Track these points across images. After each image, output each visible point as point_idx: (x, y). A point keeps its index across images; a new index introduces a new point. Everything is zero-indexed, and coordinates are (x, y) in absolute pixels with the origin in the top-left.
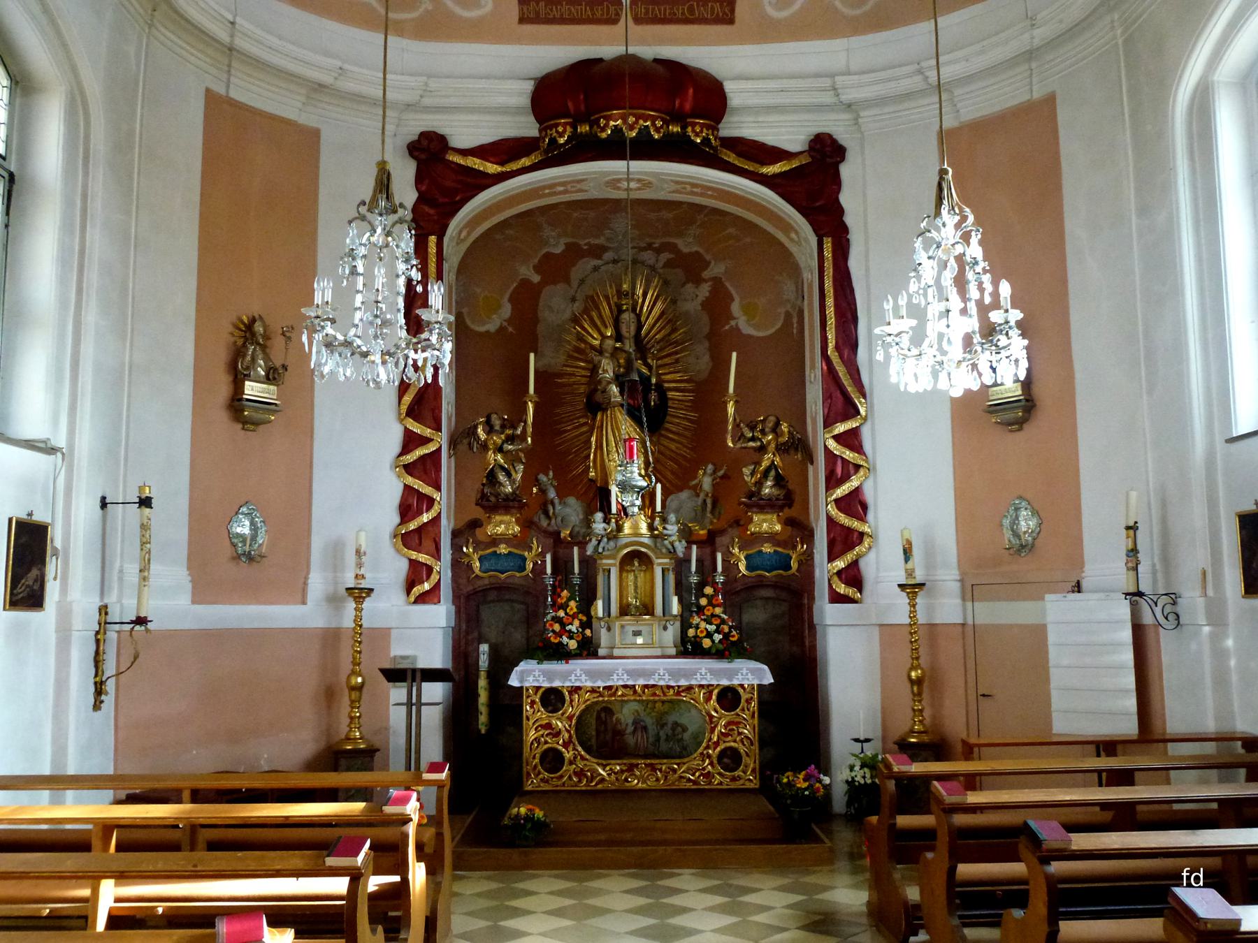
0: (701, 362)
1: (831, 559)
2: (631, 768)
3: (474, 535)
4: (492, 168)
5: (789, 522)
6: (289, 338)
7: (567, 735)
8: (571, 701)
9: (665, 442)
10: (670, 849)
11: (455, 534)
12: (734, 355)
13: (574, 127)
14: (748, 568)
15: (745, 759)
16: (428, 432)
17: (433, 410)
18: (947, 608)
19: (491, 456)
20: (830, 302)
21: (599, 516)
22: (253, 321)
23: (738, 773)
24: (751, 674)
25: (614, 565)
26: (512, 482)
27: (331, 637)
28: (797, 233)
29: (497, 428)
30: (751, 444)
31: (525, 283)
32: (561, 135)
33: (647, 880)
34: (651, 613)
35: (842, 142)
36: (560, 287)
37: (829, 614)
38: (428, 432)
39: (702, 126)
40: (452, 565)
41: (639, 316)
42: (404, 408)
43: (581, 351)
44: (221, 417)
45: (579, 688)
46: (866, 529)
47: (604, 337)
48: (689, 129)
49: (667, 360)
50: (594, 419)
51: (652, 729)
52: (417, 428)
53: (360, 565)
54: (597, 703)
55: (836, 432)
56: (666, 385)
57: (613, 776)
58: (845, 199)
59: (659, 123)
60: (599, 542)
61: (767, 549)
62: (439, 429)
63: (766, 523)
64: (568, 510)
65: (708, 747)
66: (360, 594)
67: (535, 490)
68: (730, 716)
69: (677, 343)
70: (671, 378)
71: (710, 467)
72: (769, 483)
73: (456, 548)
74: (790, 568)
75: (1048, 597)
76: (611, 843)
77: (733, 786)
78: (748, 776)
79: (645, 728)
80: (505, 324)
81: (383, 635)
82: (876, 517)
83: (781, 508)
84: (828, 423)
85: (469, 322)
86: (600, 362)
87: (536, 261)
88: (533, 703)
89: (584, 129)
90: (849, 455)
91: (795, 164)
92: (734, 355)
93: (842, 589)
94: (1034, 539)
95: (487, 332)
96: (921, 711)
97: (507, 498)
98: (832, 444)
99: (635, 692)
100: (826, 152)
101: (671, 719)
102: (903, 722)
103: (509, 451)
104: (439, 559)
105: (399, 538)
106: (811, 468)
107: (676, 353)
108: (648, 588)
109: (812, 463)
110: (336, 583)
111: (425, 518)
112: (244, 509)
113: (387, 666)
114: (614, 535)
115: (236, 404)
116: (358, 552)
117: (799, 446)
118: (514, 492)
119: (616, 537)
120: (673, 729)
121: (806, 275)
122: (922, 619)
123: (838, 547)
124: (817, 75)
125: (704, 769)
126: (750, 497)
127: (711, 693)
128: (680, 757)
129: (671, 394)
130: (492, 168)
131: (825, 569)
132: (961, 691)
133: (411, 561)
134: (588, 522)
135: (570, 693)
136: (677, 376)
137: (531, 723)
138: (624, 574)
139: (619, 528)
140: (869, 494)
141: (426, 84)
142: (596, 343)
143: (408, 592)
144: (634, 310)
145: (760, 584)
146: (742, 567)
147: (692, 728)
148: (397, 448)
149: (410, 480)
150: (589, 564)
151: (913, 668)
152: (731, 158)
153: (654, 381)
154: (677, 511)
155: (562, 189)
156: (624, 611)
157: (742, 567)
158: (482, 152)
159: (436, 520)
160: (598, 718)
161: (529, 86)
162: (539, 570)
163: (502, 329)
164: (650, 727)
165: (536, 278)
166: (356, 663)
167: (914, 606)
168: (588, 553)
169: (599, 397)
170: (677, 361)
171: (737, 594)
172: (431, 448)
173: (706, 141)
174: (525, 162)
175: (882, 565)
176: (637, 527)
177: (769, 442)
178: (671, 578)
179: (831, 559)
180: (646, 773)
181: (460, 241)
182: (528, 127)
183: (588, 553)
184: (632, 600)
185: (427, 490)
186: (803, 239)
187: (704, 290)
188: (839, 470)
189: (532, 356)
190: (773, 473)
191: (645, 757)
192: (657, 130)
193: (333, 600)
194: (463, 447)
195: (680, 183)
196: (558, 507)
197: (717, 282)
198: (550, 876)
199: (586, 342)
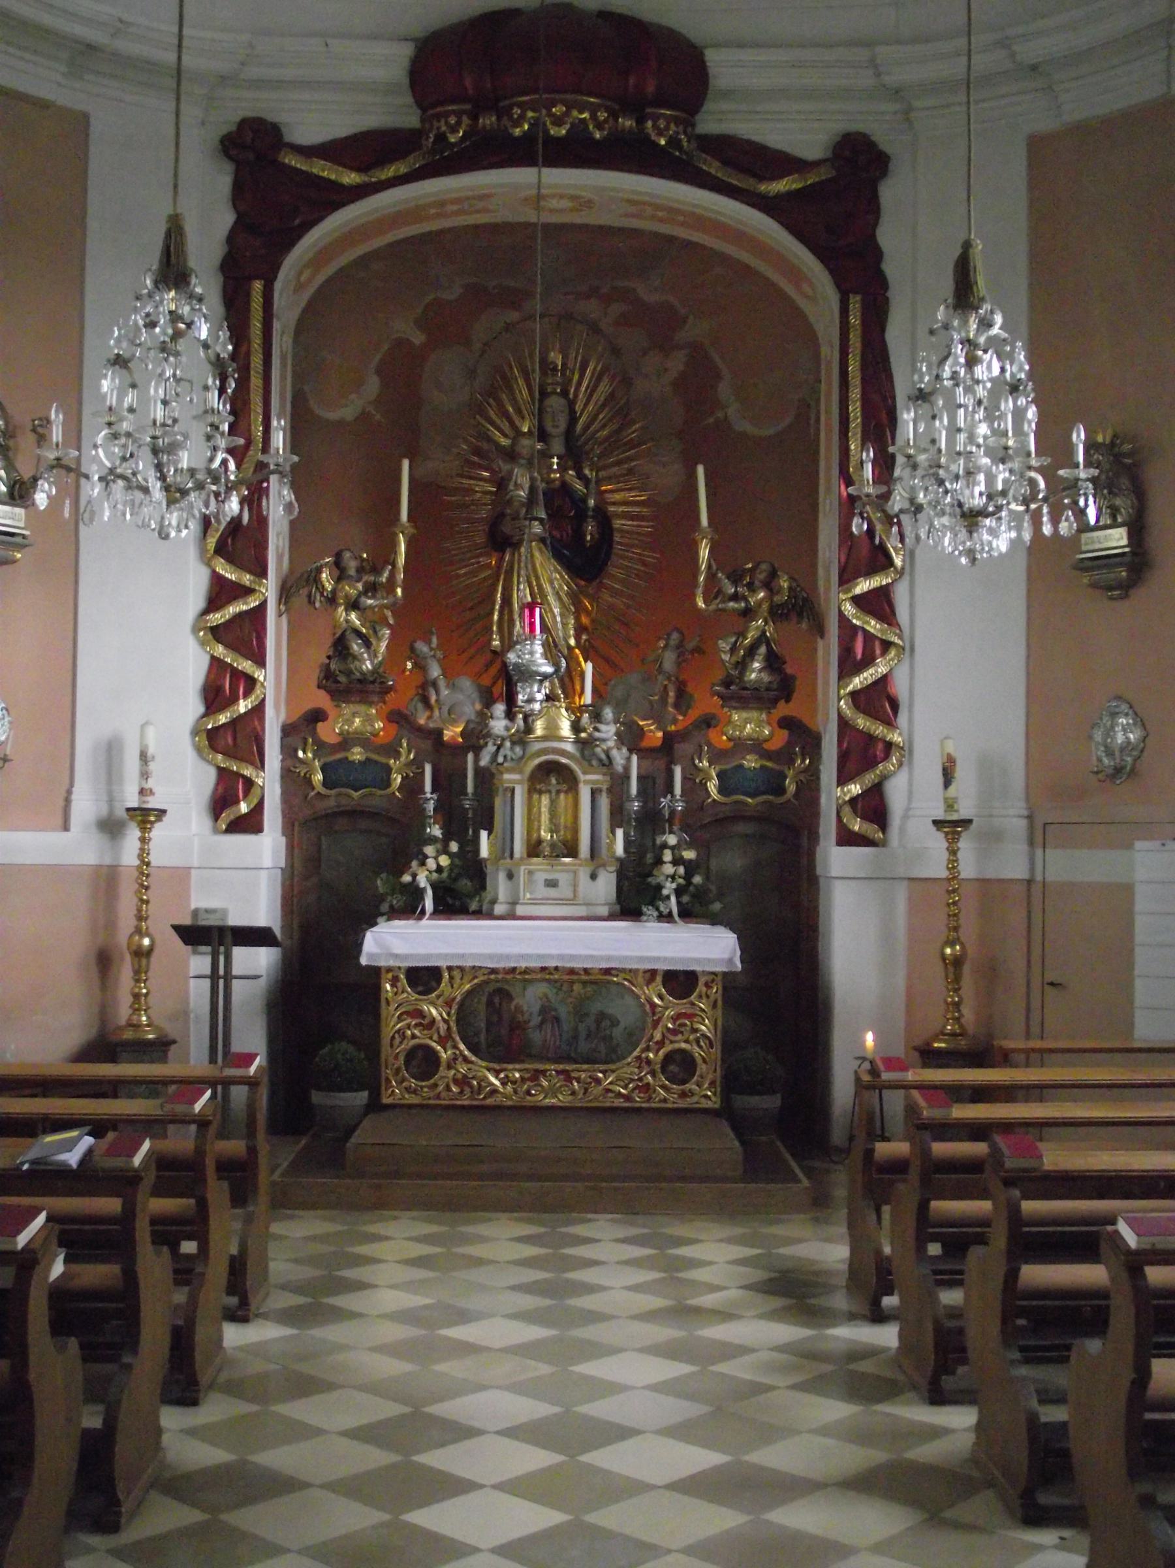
1: (842, 780)
2: (536, 1075)
3: (314, 733)
4: (350, 178)
7: (443, 1027)
10: (579, 1185)
11: (288, 731)
12: (700, 470)
13: (475, 118)
14: (721, 790)
15: (702, 1068)
16: (247, 579)
20: (855, 393)
21: (500, 708)
23: (691, 1086)
24: (712, 947)
25: (518, 782)
26: (372, 663)
27: (106, 880)
28: (811, 284)
29: (352, 572)
30: (731, 604)
31: (400, 343)
32: (454, 130)
33: (545, 1226)
34: (572, 852)
35: (885, 147)
37: (837, 861)
38: (247, 579)
39: (669, 119)
40: (282, 777)
41: (571, 404)
42: (212, 542)
43: (484, 452)
46: (896, 738)
47: (519, 433)
48: (649, 124)
50: (501, 559)
52: (231, 575)
53: (145, 775)
56: (612, 509)
57: (509, 1088)
58: (888, 236)
59: (602, 115)
62: (262, 573)
63: (748, 724)
64: (460, 697)
65: (648, 1049)
66: (146, 817)
67: (409, 665)
68: (681, 1006)
69: (632, 445)
72: (756, 665)
73: (288, 752)
74: (782, 790)
75: (1139, 845)
76: (499, 1176)
77: (682, 1104)
78: (704, 1092)
79: (557, 1019)
80: (371, 409)
82: (911, 721)
84: (847, 578)
85: (313, 404)
86: (510, 473)
89: (488, 121)
90: (873, 626)
92: (700, 470)
94: (1136, 760)
95: (341, 423)
96: (957, 1006)
97: (363, 680)
98: (849, 609)
100: (859, 166)
101: (596, 1007)
102: (936, 1023)
103: (371, 607)
105: (204, 736)
106: (821, 644)
107: (630, 459)
108: (570, 820)
109: (822, 637)
110: (111, 800)
111: (243, 706)
113: (187, 921)
114: (522, 738)
116: (144, 757)
117: (801, 609)
118: (375, 671)
120: (598, 1022)
121: (825, 350)
122: (968, 870)
123: (850, 766)
124: (851, 43)
129: (617, 523)
130: (350, 178)
131: (836, 794)
134: (484, 717)
136: (631, 496)
137: (393, 1006)
138: (536, 796)
139: (529, 729)
140: (900, 687)
141: (251, 46)
142: (504, 442)
143: (216, 816)
144: (565, 393)
145: (739, 815)
146: (712, 786)
149: (220, 650)
150: (486, 778)
151: (952, 944)
152: (713, 167)
153: (592, 502)
154: (619, 707)
155: (455, 208)
156: (534, 848)
157: (712, 786)
158: (331, 151)
159: (258, 710)
160: (490, 1003)
161: (406, 51)
162: (412, 786)
163: (363, 417)
165: (418, 338)
166: (140, 918)
169: (507, 528)
170: (630, 471)
171: (703, 825)
172: (253, 602)
173: (674, 142)
175: (913, 793)
177: (759, 604)
178: (604, 802)
180: (559, 1082)
181: (300, 287)
182: (401, 114)
184: (546, 835)
185: (246, 665)
186: (819, 295)
187: (677, 363)
189: (406, 464)
190: (763, 650)
191: (557, 1061)
192: (599, 126)
193: (110, 827)
194: (299, 600)
195: (636, 204)
196: (445, 692)
198: (413, 1218)
199: (489, 440)
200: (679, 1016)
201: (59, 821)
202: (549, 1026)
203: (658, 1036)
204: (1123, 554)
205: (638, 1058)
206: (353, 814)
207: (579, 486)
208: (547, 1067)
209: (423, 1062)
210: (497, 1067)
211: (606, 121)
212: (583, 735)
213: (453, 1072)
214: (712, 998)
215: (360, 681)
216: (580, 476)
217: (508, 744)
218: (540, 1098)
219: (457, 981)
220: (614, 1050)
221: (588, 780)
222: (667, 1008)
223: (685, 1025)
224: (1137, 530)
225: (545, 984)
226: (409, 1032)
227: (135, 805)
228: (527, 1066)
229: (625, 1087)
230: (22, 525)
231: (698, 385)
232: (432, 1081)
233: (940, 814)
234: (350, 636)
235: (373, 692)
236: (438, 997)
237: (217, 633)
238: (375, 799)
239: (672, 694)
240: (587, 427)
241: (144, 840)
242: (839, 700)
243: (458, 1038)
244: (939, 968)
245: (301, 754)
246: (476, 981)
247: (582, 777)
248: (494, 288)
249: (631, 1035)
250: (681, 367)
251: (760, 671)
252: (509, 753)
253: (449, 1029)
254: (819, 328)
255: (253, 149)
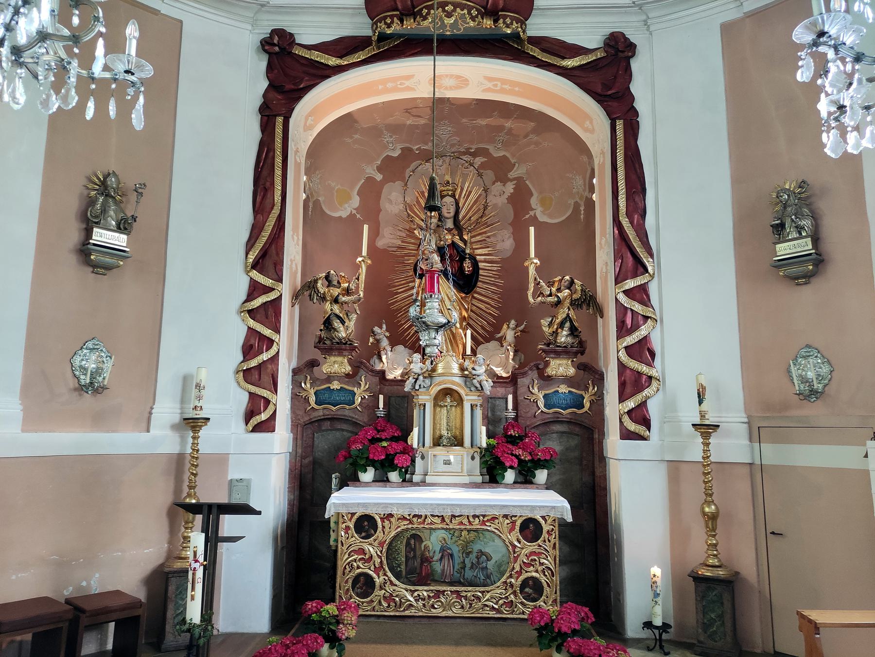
0: (506, 243)
4: (333, 61)
5: (583, 367)
6: (141, 194)
8: (383, 527)
9: (475, 302)
11: (296, 372)
15: (547, 590)
17: (275, 265)
18: (732, 446)
19: (328, 306)
22: (107, 176)
25: (427, 400)
26: (347, 329)
29: (335, 283)
30: (550, 299)
31: (370, 180)
34: (460, 443)
36: (399, 184)
37: (614, 445)
44: (73, 259)
45: (391, 515)
46: (653, 372)
48: (501, 21)
49: (478, 238)
51: (458, 557)
54: (407, 530)
55: (627, 287)
58: (637, 88)
59: (474, 12)
60: (417, 379)
61: (563, 389)
62: (280, 280)
63: (561, 367)
65: (511, 576)
66: (193, 424)
68: (532, 547)
70: (481, 253)
71: (513, 323)
72: (565, 333)
73: (296, 384)
79: (452, 555)
80: (354, 212)
81: (221, 460)
83: (576, 354)
87: (379, 162)
88: (347, 528)
90: (638, 307)
91: (591, 58)
93: (632, 427)
96: (715, 545)
98: (622, 298)
99: (443, 520)
100: (619, 51)
101: (476, 547)
104: (276, 391)
106: (600, 320)
107: (485, 233)
108: (458, 421)
111: (265, 356)
112: (90, 345)
114: (431, 374)
115: (84, 250)
117: (588, 302)
119: (430, 377)
120: (478, 558)
123: (628, 390)
125: (507, 598)
126: (548, 345)
127: (514, 523)
128: (485, 586)
129: (481, 265)
130: (333, 61)
131: (614, 409)
132: (751, 528)
133: (251, 394)
135: (382, 519)
139: (434, 370)
140: (656, 343)
143: (247, 422)
144: (453, 196)
145: (557, 420)
147: (495, 557)
148: (244, 298)
149: (252, 323)
151: (708, 503)
152: (536, 52)
156: (437, 442)
157: (541, 404)
158: (323, 47)
159: (275, 359)
160: (408, 544)
163: (351, 216)
164: (455, 555)
165: (379, 177)
167: (708, 444)
168: (406, 389)
172: (272, 296)
174: (361, 56)
176: (450, 367)
177: (566, 298)
178: (479, 413)
179: (622, 399)
183: (406, 389)
184: (444, 433)
185: (267, 332)
187: (510, 188)
188: (629, 321)
190: (568, 324)
191: (452, 584)
197: (519, 181)
200: (533, 553)
201: (144, 425)
202: (446, 558)
203: (517, 568)
204: (810, 254)
205: (505, 582)
206: (333, 419)
207: (462, 244)
208: (444, 588)
209: (364, 584)
210: (412, 588)
211: (477, 16)
212: (466, 372)
213: (383, 591)
214: (553, 541)
215: (338, 343)
216: (462, 239)
217: (421, 378)
218: (438, 612)
219: (387, 530)
220: (488, 577)
221: (470, 398)
222: (522, 548)
223: (535, 560)
224: (816, 241)
225: (443, 531)
226: (355, 564)
227: (190, 416)
228: (432, 588)
229: (496, 603)
230: (125, 245)
231: (520, 200)
232: (369, 599)
233: (697, 421)
234: (333, 318)
235: (345, 350)
236: (375, 540)
237: (251, 312)
238: (346, 411)
239: (512, 354)
240: (464, 217)
241: (194, 438)
242: (618, 352)
243: (387, 569)
244: (701, 521)
245: (303, 385)
246: (399, 529)
247: (465, 398)
248: (417, 149)
249: (500, 566)
250: (512, 191)
251: (567, 336)
252: (422, 384)
253: (381, 562)
254: (594, 149)
255: (279, 49)
